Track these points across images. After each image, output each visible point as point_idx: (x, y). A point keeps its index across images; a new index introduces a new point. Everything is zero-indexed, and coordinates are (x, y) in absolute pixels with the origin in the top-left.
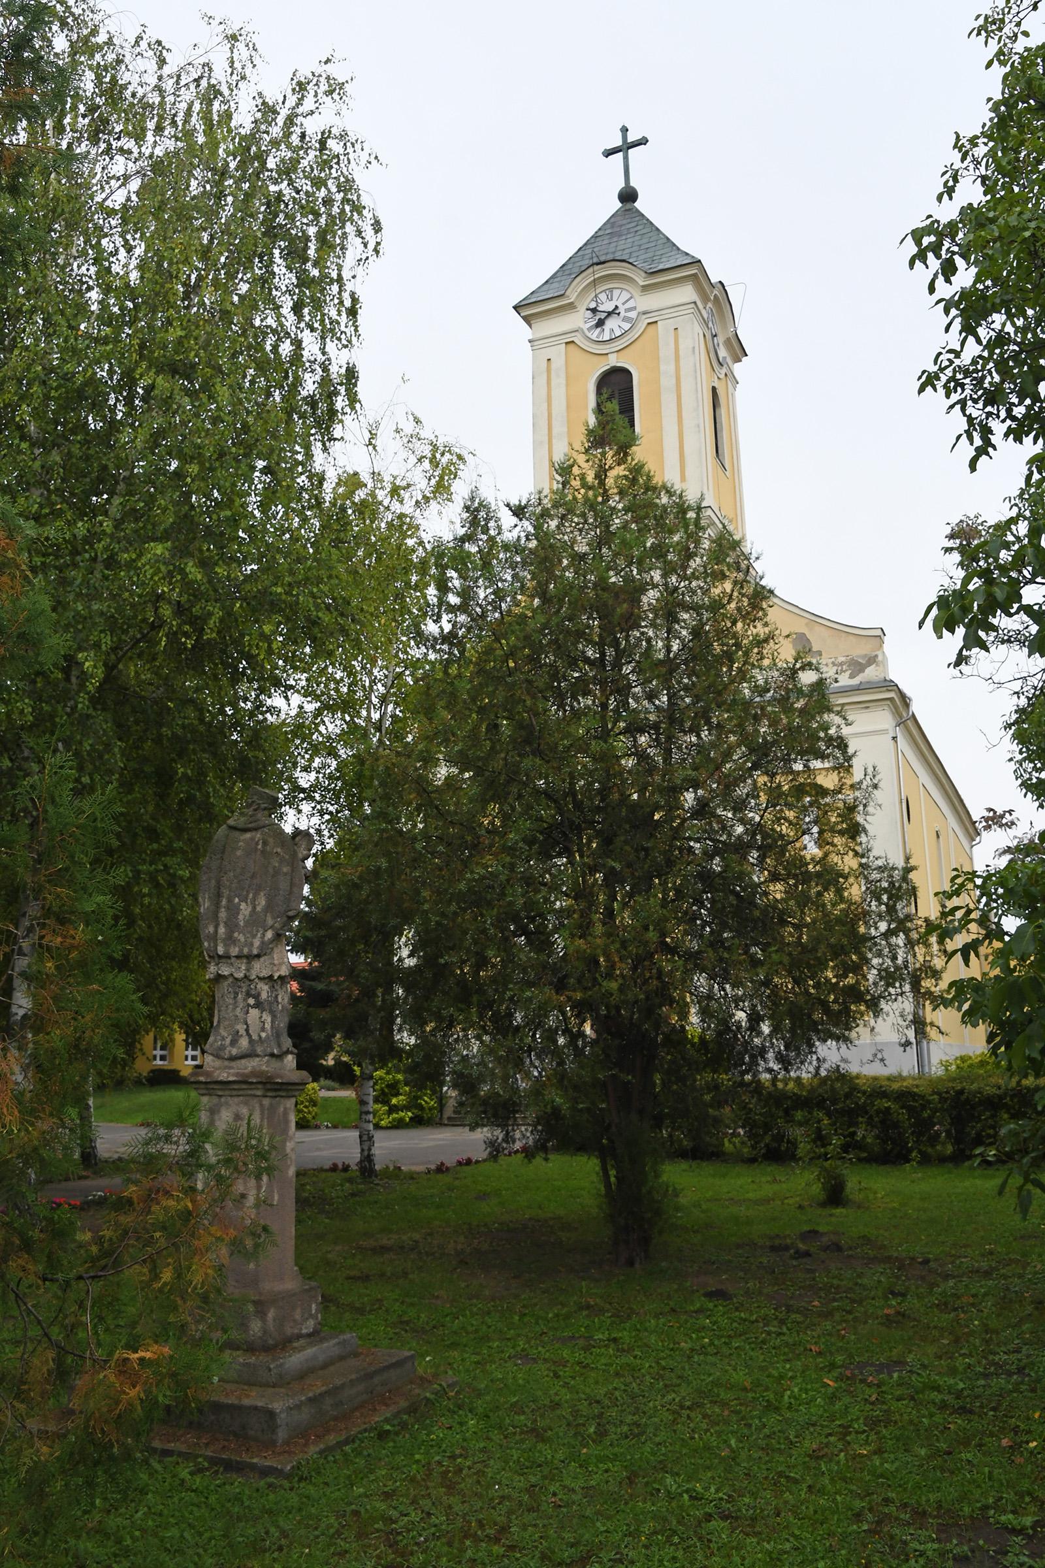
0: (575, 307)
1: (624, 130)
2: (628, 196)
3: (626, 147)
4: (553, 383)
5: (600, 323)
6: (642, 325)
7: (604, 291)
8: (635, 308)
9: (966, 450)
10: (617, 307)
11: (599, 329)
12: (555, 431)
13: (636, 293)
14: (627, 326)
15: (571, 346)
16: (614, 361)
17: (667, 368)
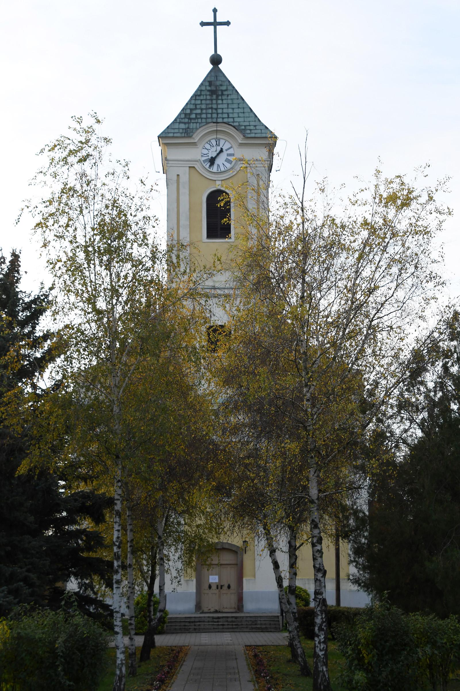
0: (196, 145)
2: (216, 60)
8: (233, 155)
12: (181, 223)
15: (192, 169)
16: (218, 186)
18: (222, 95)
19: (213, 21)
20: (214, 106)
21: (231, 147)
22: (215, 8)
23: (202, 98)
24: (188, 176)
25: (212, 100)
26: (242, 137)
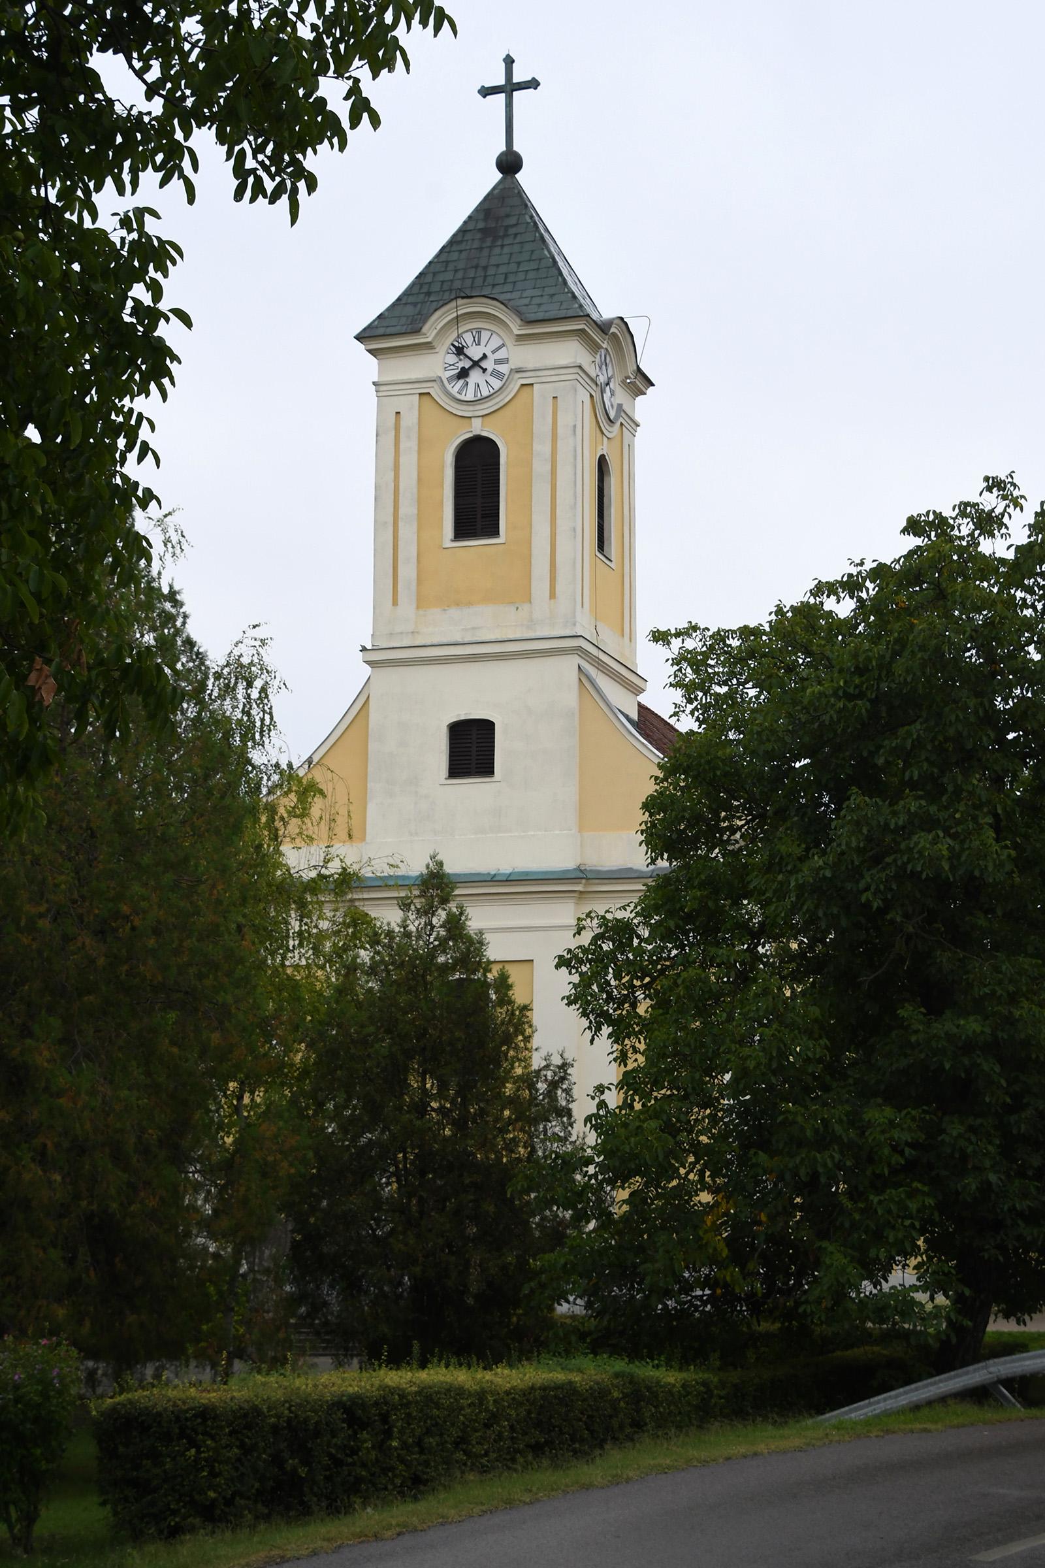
0: (433, 348)
1: (509, 61)
2: (510, 164)
3: (509, 88)
4: (402, 446)
5: (463, 374)
7: (471, 330)
9: (589, 1034)
10: (485, 357)
11: (461, 382)
15: (425, 398)
16: (477, 428)
17: (542, 448)
18: (506, 235)
19: (503, 83)
20: (483, 263)
21: (504, 345)
22: (508, 56)
23: (463, 246)
24: (416, 413)
25: (481, 249)
26: (519, 321)
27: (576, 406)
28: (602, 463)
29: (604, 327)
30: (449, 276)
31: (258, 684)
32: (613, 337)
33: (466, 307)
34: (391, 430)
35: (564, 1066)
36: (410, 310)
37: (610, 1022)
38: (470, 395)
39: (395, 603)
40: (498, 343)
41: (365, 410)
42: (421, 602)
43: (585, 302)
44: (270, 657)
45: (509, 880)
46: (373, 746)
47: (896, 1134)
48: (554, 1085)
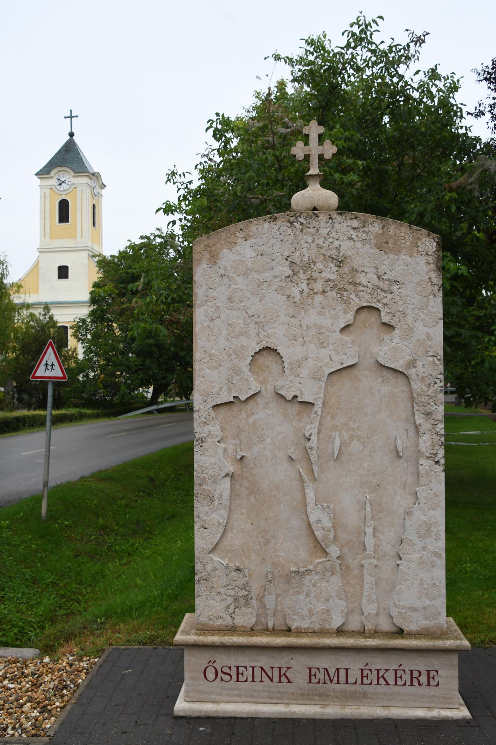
1: (71, 111)
2: (71, 135)
3: (71, 117)
5: (60, 184)
6: (72, 188)
13: (71, 177)
14: (68, 187)
16: (64, 197)
17: (79, 202)
27: (87, 193)
28: (94, 206)
29: (93, 174)
30: (57, 161)
31: (5, 265)
32: (95, 176)
33: (60, 168)
34: (43, 197)
35: (76, 348)
36: (47, 169)
37: (82, 340)
38: (62, 189)
39: (45, 238)
40: (68, 176)
41: (37, 192)
42: (51, 238)
43: (88, 168)
44: (7, 259)
45: (72, 303)
46: (40, 271)
47: (136, 363)
48: (73, 352)
